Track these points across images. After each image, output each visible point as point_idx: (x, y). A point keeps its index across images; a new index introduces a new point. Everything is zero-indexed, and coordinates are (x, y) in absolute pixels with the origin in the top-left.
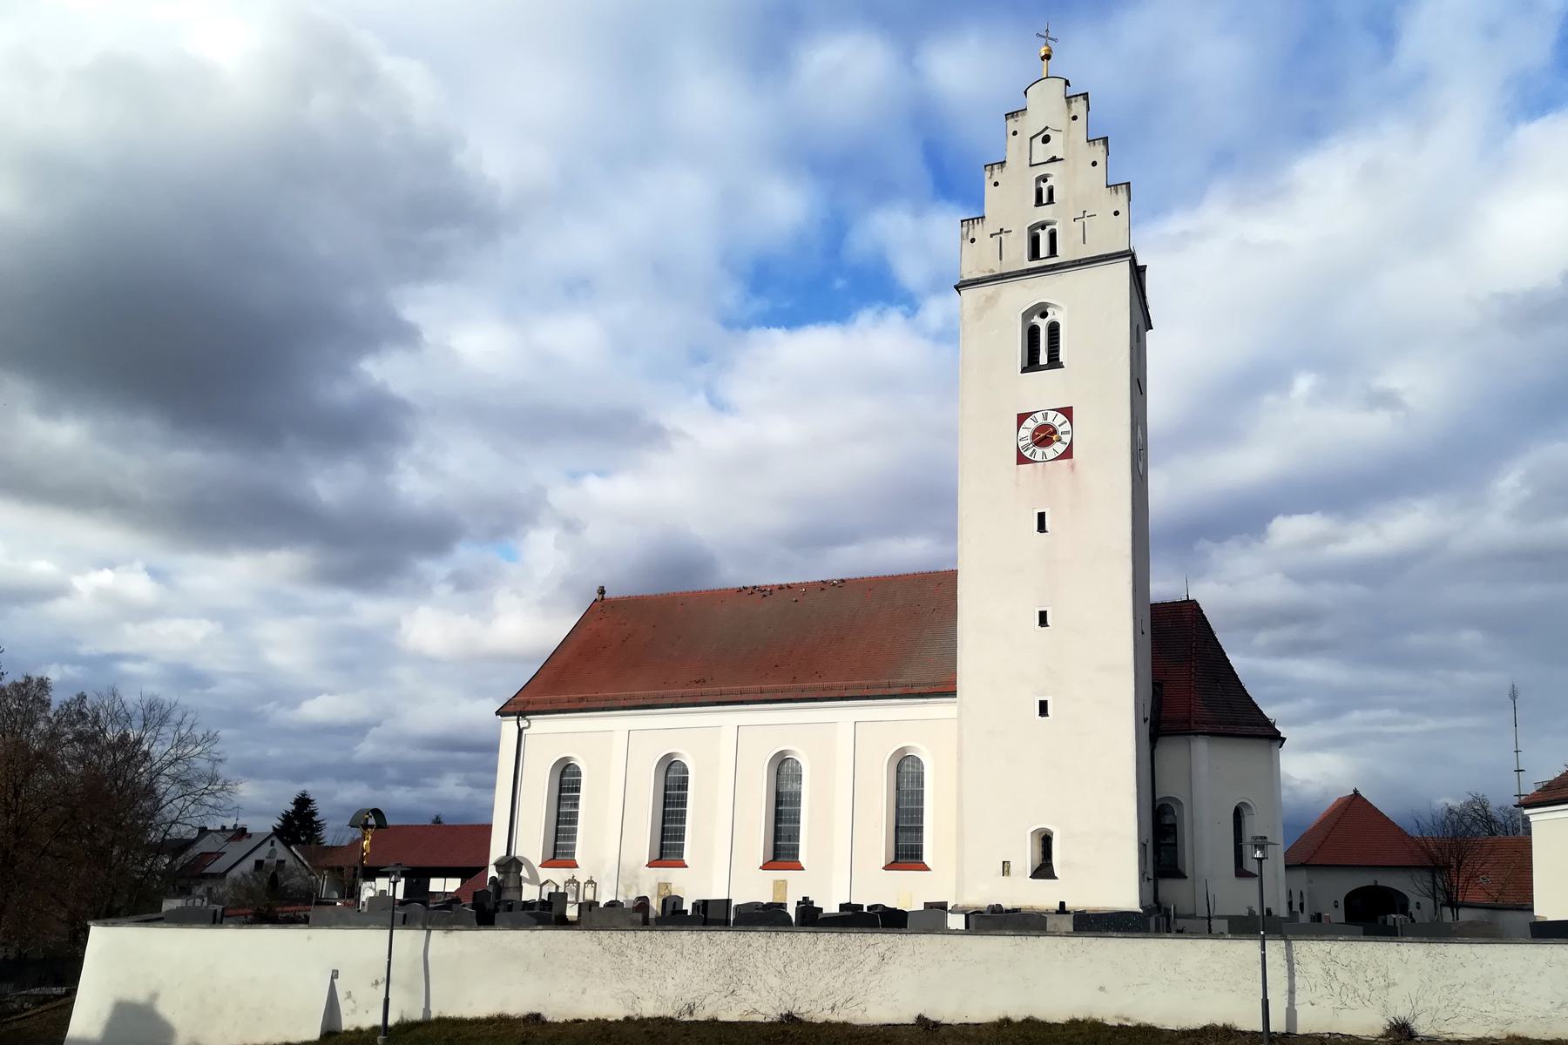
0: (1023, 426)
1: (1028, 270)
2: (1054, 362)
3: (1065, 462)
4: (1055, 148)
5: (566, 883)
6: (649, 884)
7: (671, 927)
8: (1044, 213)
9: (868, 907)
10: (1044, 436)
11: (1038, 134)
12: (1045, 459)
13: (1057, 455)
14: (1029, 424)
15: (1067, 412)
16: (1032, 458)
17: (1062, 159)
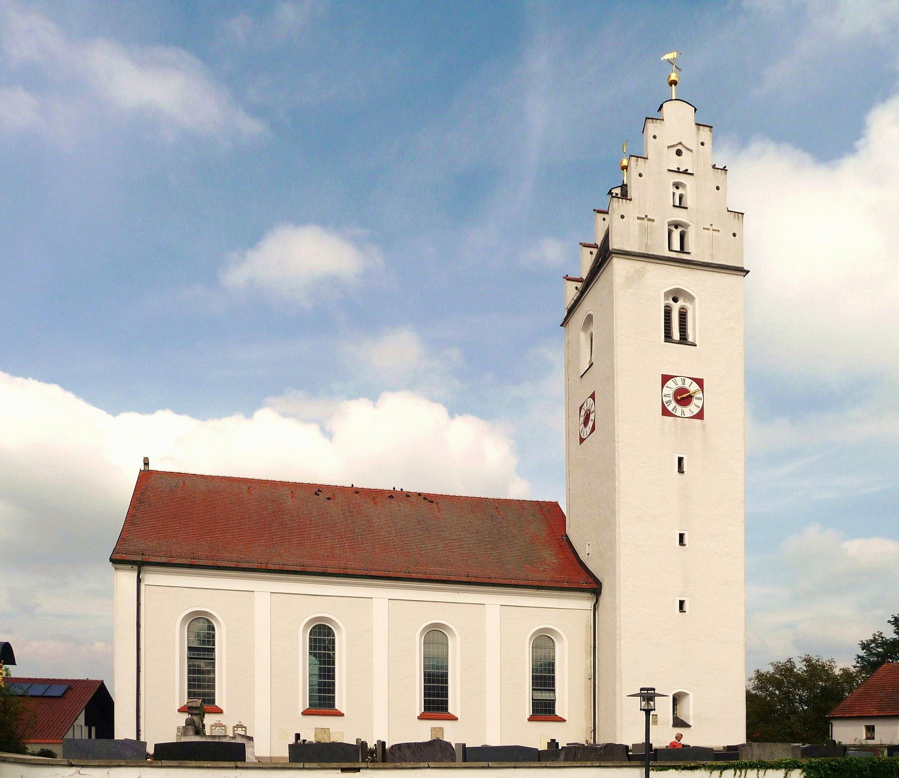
0: (666, 385)
1: (669, 257)
2: (683, 340)
3: (697, 421)
4: (685, 162)
5: (234, 727)
6: (423, 732)
7: (315, 765)
8: (680, 216)
9: (157, 746)
10: (683, 398)
11: (674, 146)
12: (683, 416)
13: (693, 415)
14: (694, 387)
15: (665, 379)
16: (674, 413)
17: (692, 174)
